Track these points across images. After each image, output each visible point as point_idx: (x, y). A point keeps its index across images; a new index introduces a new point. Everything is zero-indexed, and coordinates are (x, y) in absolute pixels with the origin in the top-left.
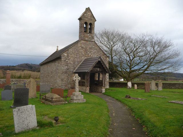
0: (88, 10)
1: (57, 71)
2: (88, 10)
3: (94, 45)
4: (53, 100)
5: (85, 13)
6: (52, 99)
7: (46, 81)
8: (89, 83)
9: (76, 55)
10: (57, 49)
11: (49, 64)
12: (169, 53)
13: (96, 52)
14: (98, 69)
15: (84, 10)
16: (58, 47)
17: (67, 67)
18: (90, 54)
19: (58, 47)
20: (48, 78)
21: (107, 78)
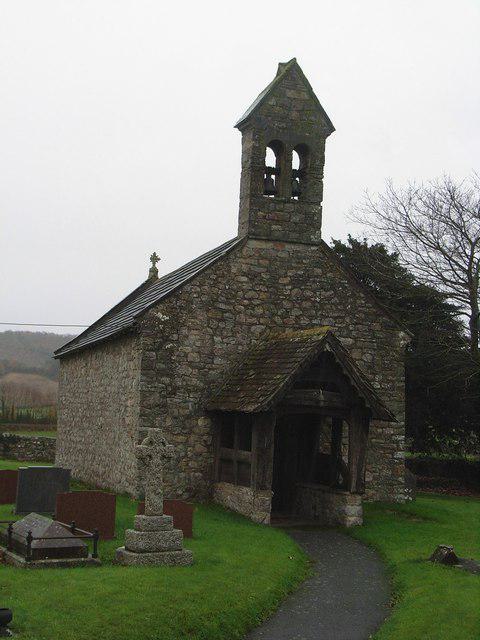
0: (290, 76)
1: (123, 398)
2: (290, 76)
3: (318, 265)
4: (34, 544)
5: (274, 90)
6: (30, 539)
7: (79, 446)
8: (269, 472)
9: (220, 320)
10: (154, 271)
11: (93, 361)
12: (47, 450)
13: (329, 299)
14: (322, 397)
15: (269, 76)
16: (155, 259)
17: (167, 380)
18: (296, 312)
19: (155, 259)
20: (89, 432)
21: (397, 442)
